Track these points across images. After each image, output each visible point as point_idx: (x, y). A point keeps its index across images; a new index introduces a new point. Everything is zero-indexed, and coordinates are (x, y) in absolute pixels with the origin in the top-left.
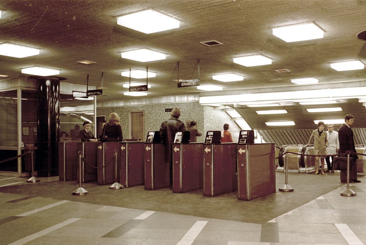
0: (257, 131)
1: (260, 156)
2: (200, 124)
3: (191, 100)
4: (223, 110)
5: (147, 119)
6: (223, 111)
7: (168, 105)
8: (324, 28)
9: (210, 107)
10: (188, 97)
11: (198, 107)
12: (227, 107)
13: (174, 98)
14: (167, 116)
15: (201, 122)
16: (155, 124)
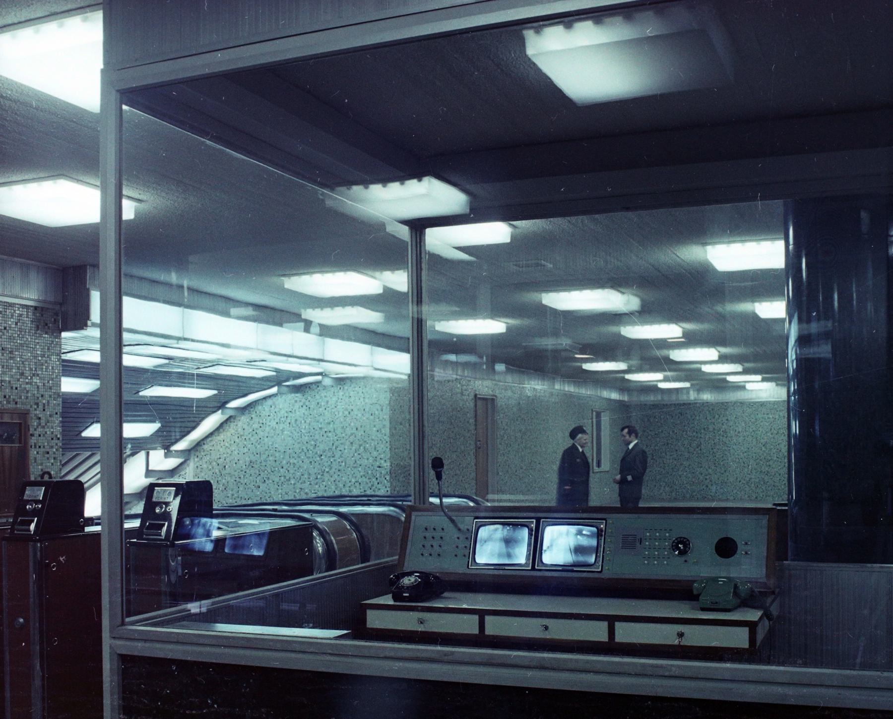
2: (43, 422)
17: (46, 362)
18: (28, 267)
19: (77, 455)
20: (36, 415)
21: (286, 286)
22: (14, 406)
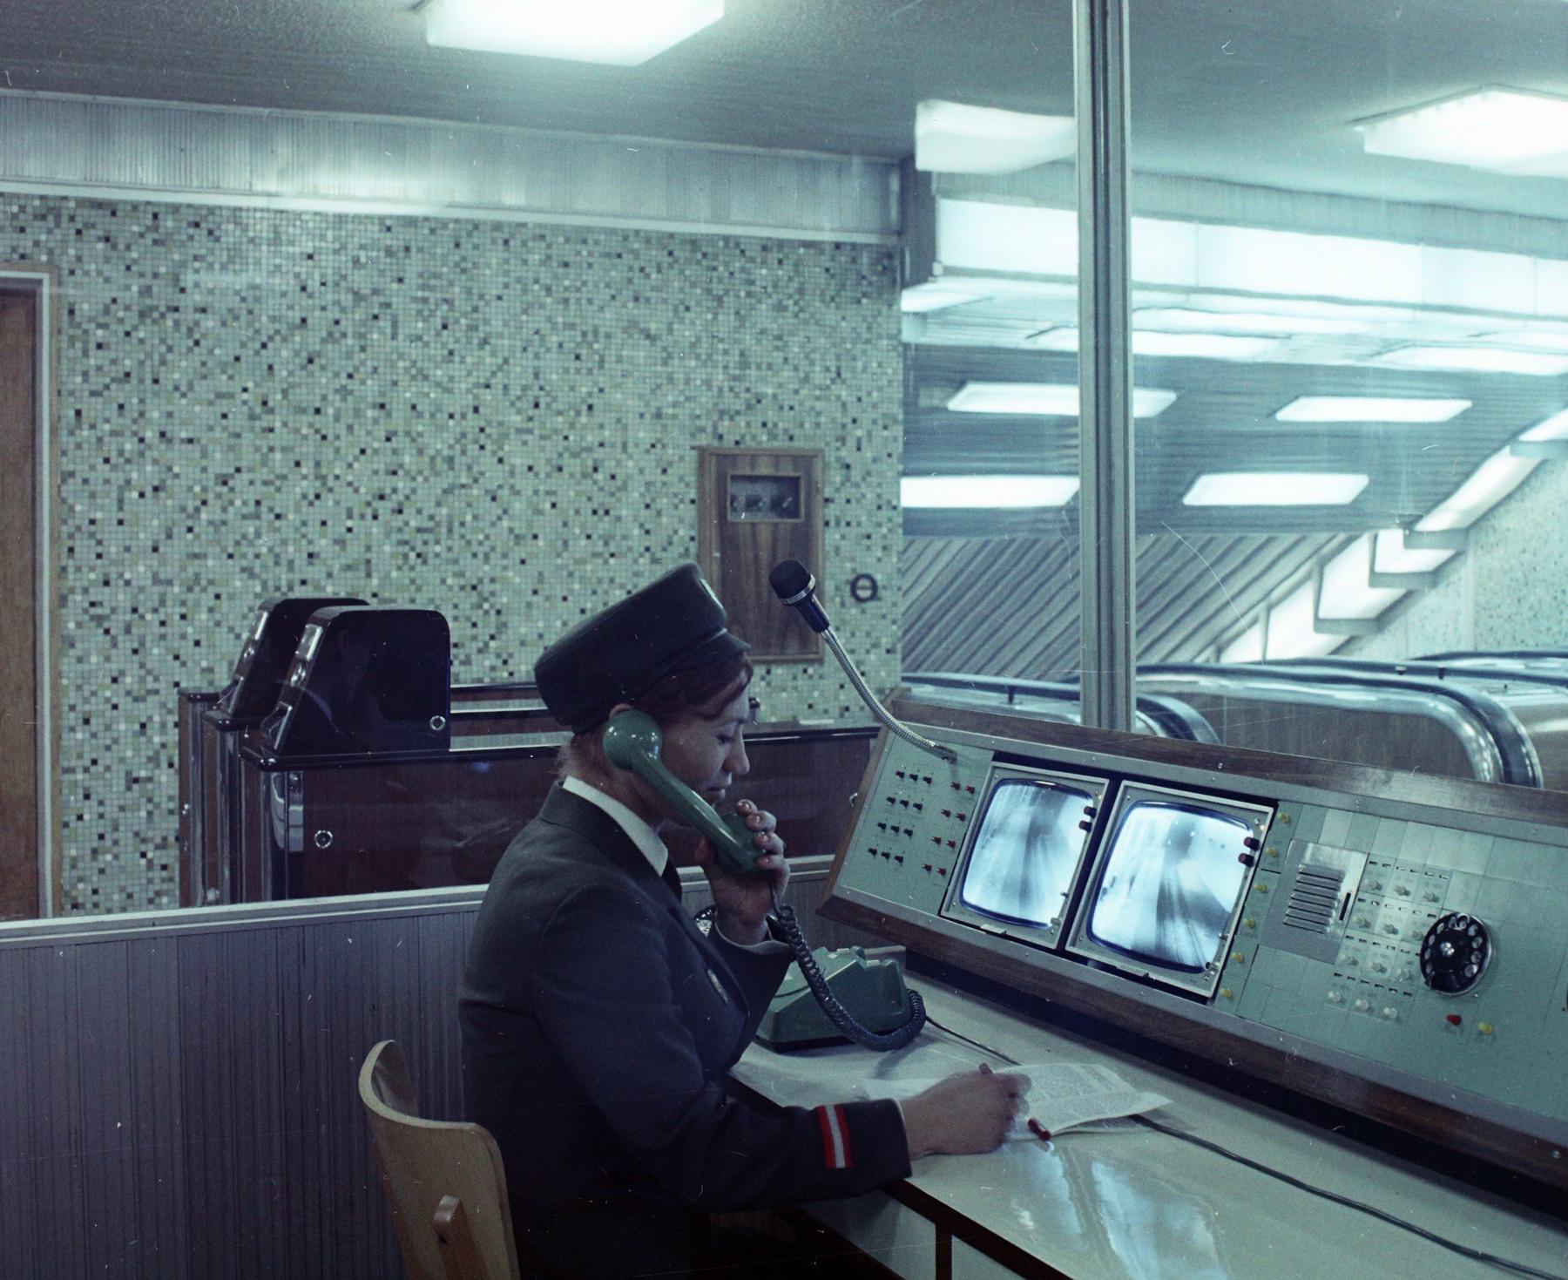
2: (856, 475)
5: (97, 382)
16: (248, 458)
17: (864, 352)
18: (815, 165)
19: (1269, 541)
20: (838, 459)
21: (1370, 148)
22: (787, 444)
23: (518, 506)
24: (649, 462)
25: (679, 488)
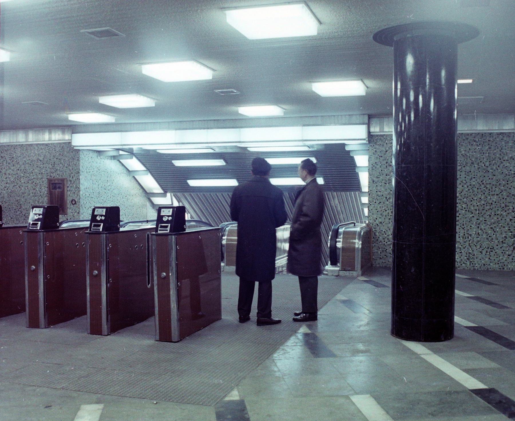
0: (172, 194)
1: (337, 396)
2: (72, 182)
3: (57, 139)
4: (114, 157)
6: (114, 159)
7: (13, 148)
8: (319, 16)
9: (90, 152)
10: (50, 133)
11: (73, 153)
12: (121, 152)
13: (24, 135)
14: (12, 168)
15: (74, 179)
23: (23, 188)
24: (41, 181)
25: (45, 185)
